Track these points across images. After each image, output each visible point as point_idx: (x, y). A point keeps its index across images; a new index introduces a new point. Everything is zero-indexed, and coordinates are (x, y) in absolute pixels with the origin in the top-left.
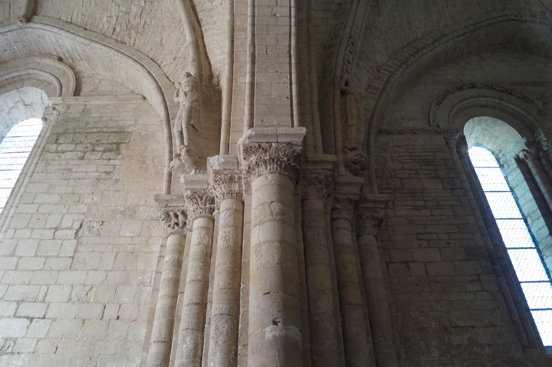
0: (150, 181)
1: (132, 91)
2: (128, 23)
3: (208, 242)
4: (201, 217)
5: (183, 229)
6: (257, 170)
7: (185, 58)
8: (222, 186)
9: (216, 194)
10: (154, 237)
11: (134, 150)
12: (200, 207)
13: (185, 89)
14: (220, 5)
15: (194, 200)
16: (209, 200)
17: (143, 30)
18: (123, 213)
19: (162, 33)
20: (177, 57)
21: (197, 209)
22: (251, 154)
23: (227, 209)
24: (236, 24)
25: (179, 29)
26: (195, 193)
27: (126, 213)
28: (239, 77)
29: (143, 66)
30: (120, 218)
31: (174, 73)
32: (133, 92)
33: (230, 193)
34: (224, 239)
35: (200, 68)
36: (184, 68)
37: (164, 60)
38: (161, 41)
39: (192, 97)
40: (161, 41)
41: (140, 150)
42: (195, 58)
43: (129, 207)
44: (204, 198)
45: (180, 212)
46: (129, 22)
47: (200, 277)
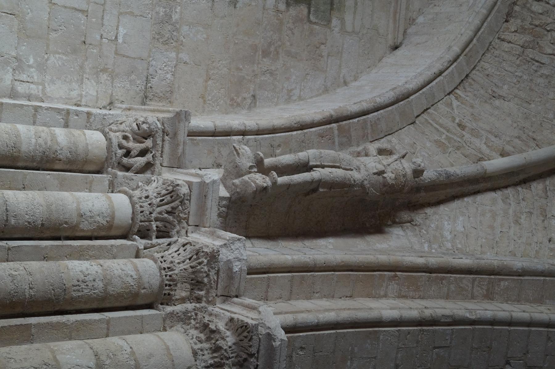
0: (225, 69)
1: (414, 20)
2: (546, 29)
3: (83, 230)
4: (133, 212)
5: (116, 165)
6: (206, 345)
7: (458, 148)
8: (187, 265)
9: (175, 242)
10: (112, 83)
11: (293, 34)
12: (154, 210)
13: (390, 170)
14: (549, 237)
15: (168, 198)
16: (165, 227)
17: (528, 59)
18: (167, 19)
19: (516, 99)
20: (463, 130)
21: (150, 204)
22: (239, 335)
23: (140, 278)
24: (503, 279)
25: (519, 138)
26: (181, 202)
27: (167, 24)
28: (397, 284)
29: (455, 60)
30: (157, 13)
31: (431, 125)
32: (412, 21)
33: (171, 283)
34: (80, 279)
35: (433, 186)
36: (440, 146)
37: (462, 103)
38: (500, 97)
39: (373, 185)
40: (500, 97)
41: (291, 45)
42: (453, 177)
43: (177, 30)
44: (171, 218)
45: (151, 159)
46: (548, 31)
47: (13, 221)
